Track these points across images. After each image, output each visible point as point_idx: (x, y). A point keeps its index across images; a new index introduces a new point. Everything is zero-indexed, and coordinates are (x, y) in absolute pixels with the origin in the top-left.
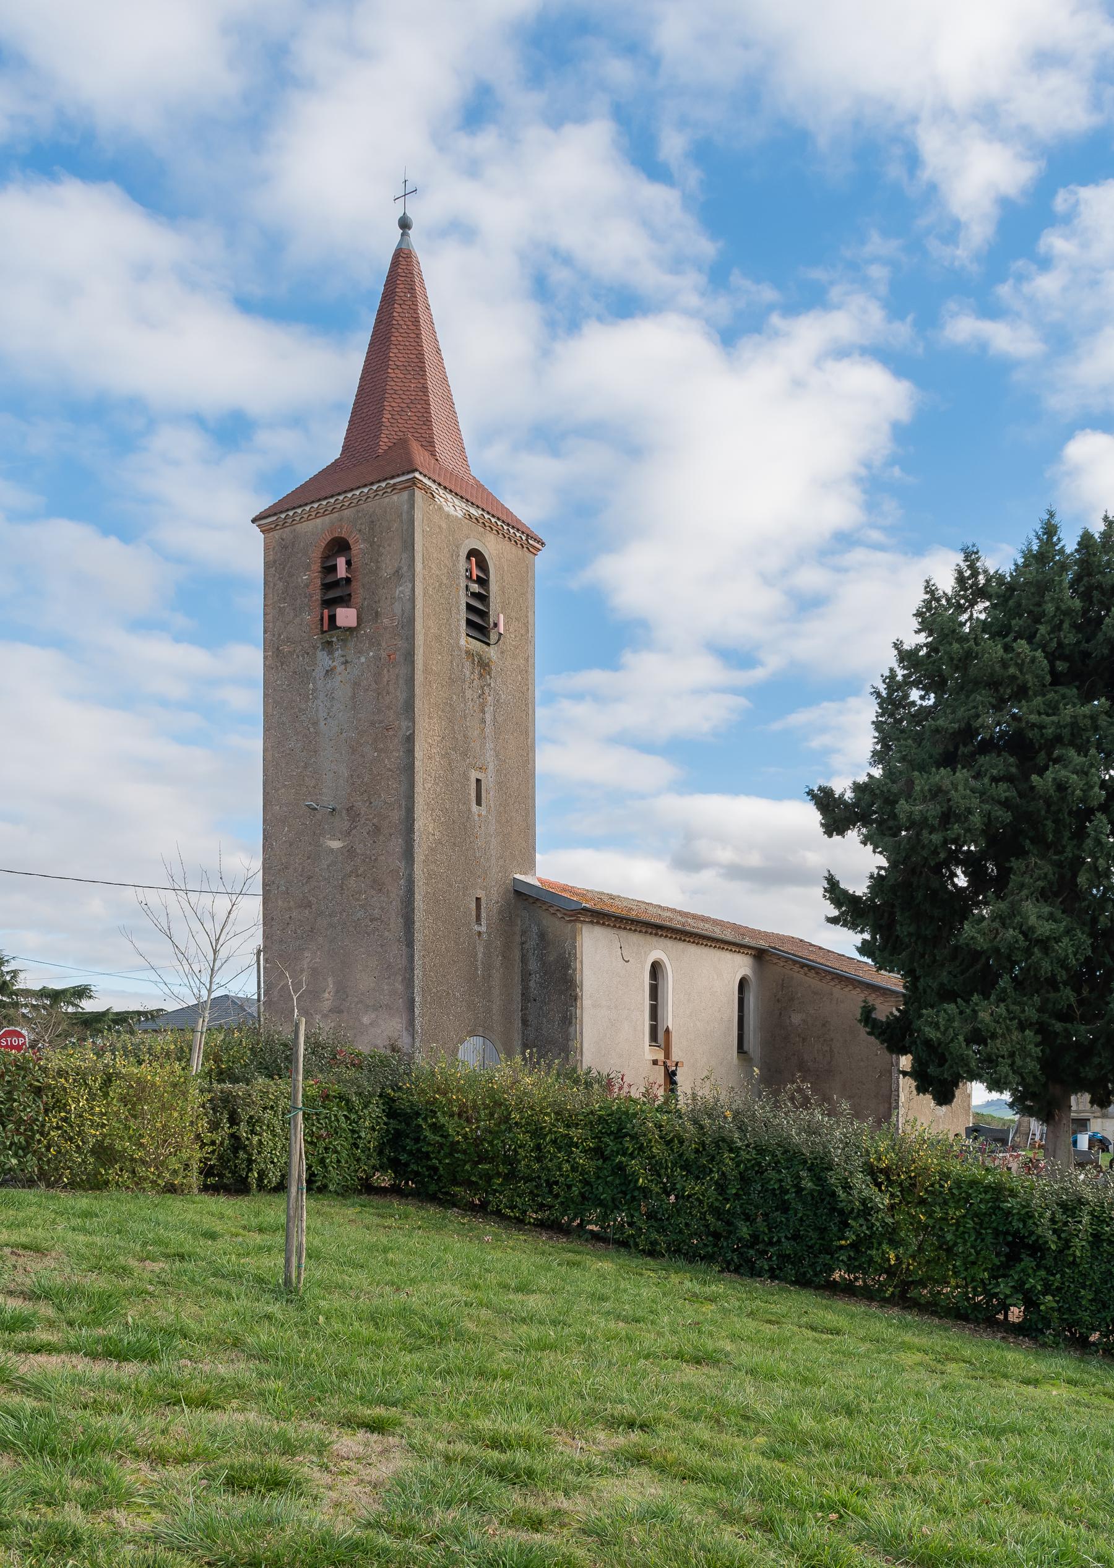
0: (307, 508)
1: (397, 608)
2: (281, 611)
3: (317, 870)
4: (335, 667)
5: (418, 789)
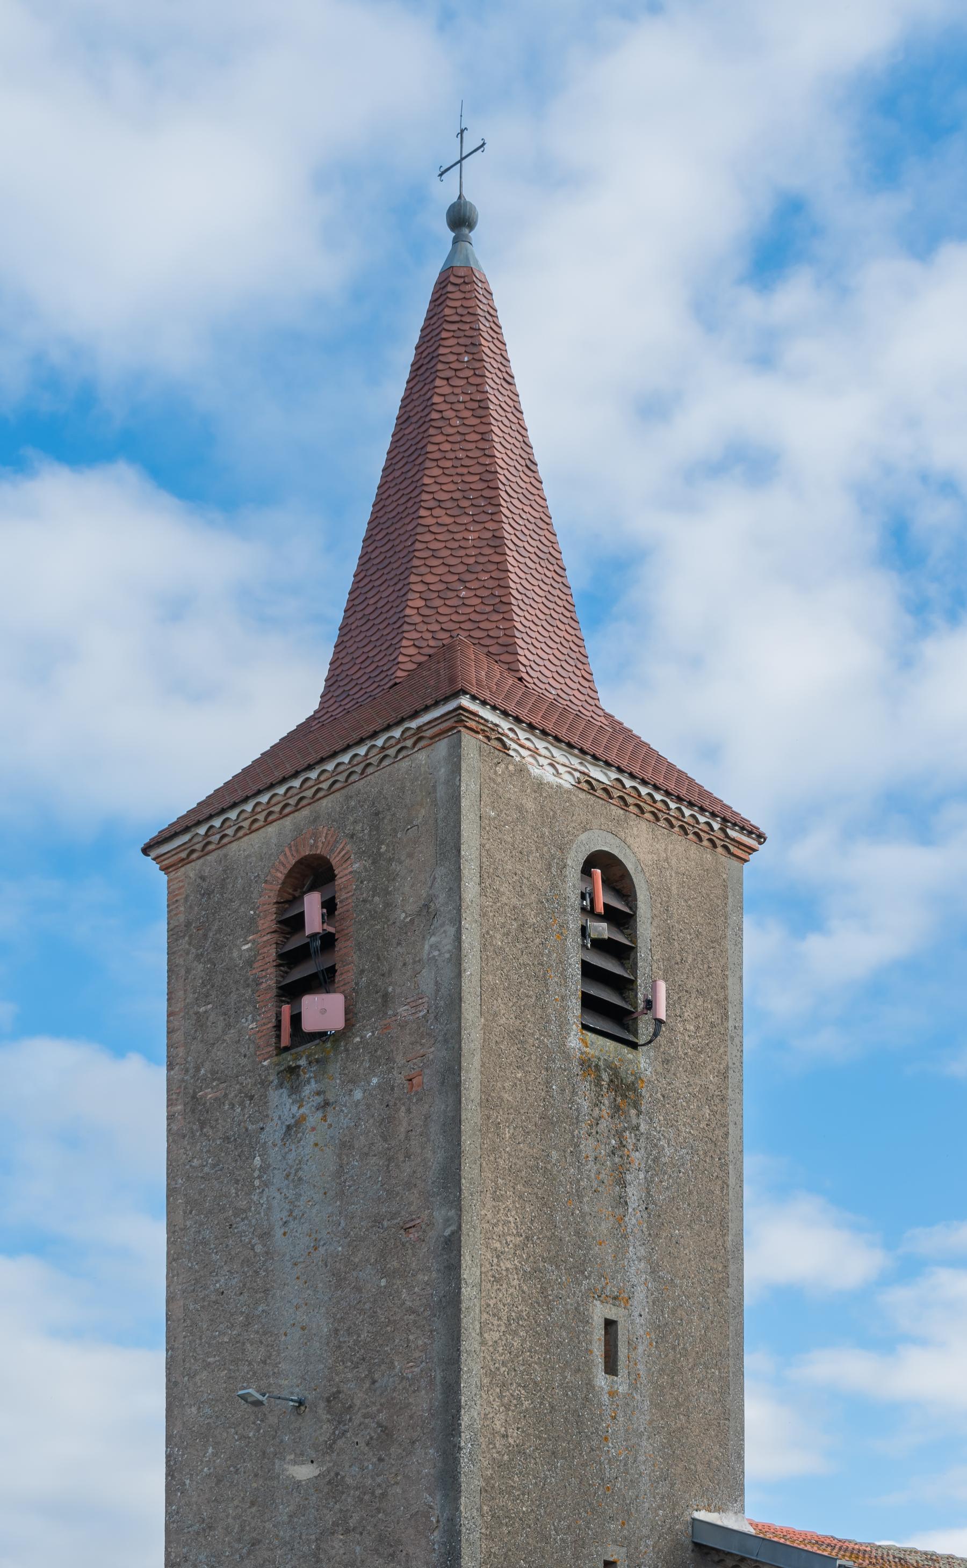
0: (249, 807)
1: (427, 980)
2: (200, 1021)
3: (269, 1525)
4: (304, 1118)
5: (470, 1342)
